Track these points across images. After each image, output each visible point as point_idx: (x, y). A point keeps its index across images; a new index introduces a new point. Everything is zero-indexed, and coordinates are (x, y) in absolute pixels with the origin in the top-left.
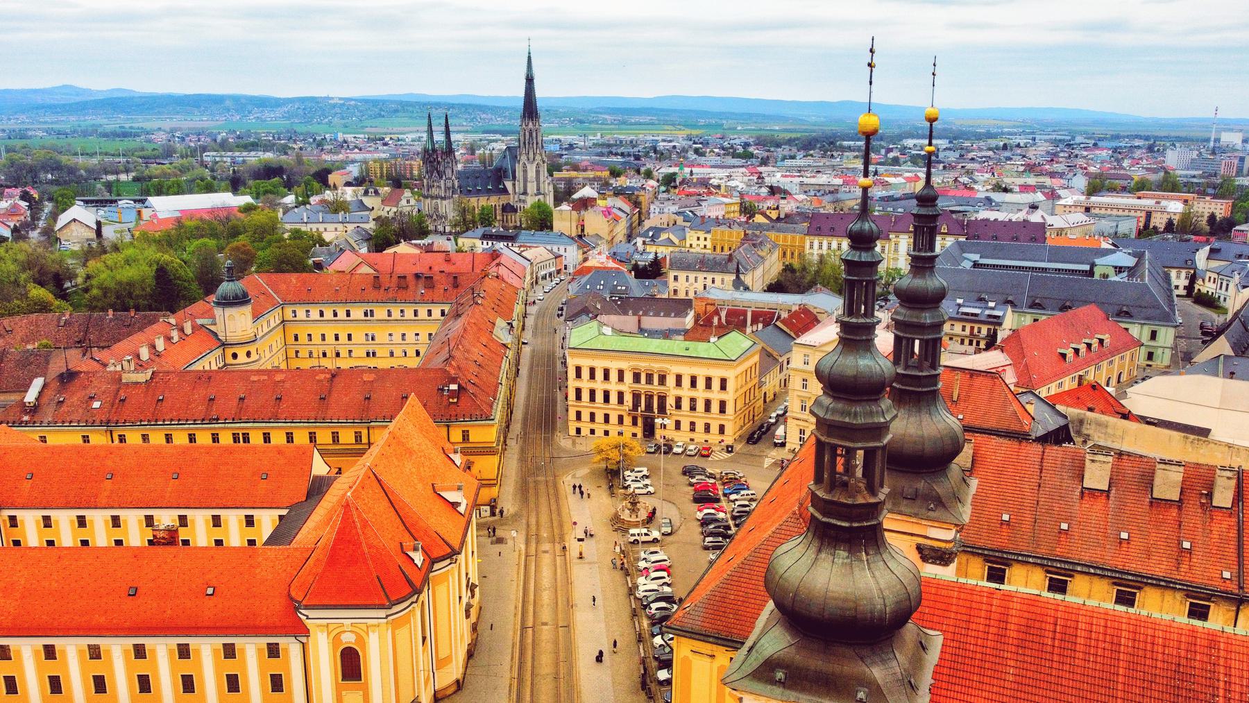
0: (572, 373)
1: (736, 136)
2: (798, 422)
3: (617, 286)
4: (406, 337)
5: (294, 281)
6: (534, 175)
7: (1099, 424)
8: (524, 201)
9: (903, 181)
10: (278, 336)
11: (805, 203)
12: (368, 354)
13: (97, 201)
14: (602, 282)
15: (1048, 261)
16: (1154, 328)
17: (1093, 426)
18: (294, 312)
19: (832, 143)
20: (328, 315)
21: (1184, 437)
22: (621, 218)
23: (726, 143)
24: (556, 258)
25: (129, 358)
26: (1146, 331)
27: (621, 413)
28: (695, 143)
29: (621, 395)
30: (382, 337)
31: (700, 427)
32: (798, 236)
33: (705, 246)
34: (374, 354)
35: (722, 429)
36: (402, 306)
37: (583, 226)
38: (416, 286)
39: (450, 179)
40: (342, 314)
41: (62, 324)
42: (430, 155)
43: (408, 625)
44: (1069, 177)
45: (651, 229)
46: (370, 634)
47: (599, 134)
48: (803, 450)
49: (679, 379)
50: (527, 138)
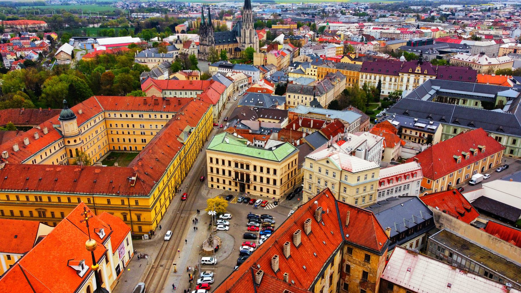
0: (208, 160)
1: (363, 3)
2: (307, 194)
3: (259, 101)
4: (158, 126)
5: (110, 100)
7: (448, 220)
8: (244, 46)
9: (430, 31)
10: (103, 124)
11: (376, 45)
12: (142, 133)
13: (80, 39)
14: (253, 99)
15: (474, 92)
16: (515, 138)
17: (445, 220)
18: (109, 114)
19: (407, 7)
20: (124, 116)
21: (489, 236)
22: (286, 54)
23: (357, 7)
24: (248, 78)
25: (5, 152)
26: (511, 140)
27: (231, 180)
28: (343, 7)
29: (230, 172)
30: (147, 126)
32: (356, 72)
33: (315, 74)
34: (144, 133)
35: (274, 192)
36: (156, 113)
37: (266, 60)
38: (163, 104)
39: (211, 37)
40: (130, 116)
41: (21, 113)
42: (202, 26)
44: (513, 29)
45: (295, 63)
47: (301, 3)
48: (264, 244)
50: (246, 17)
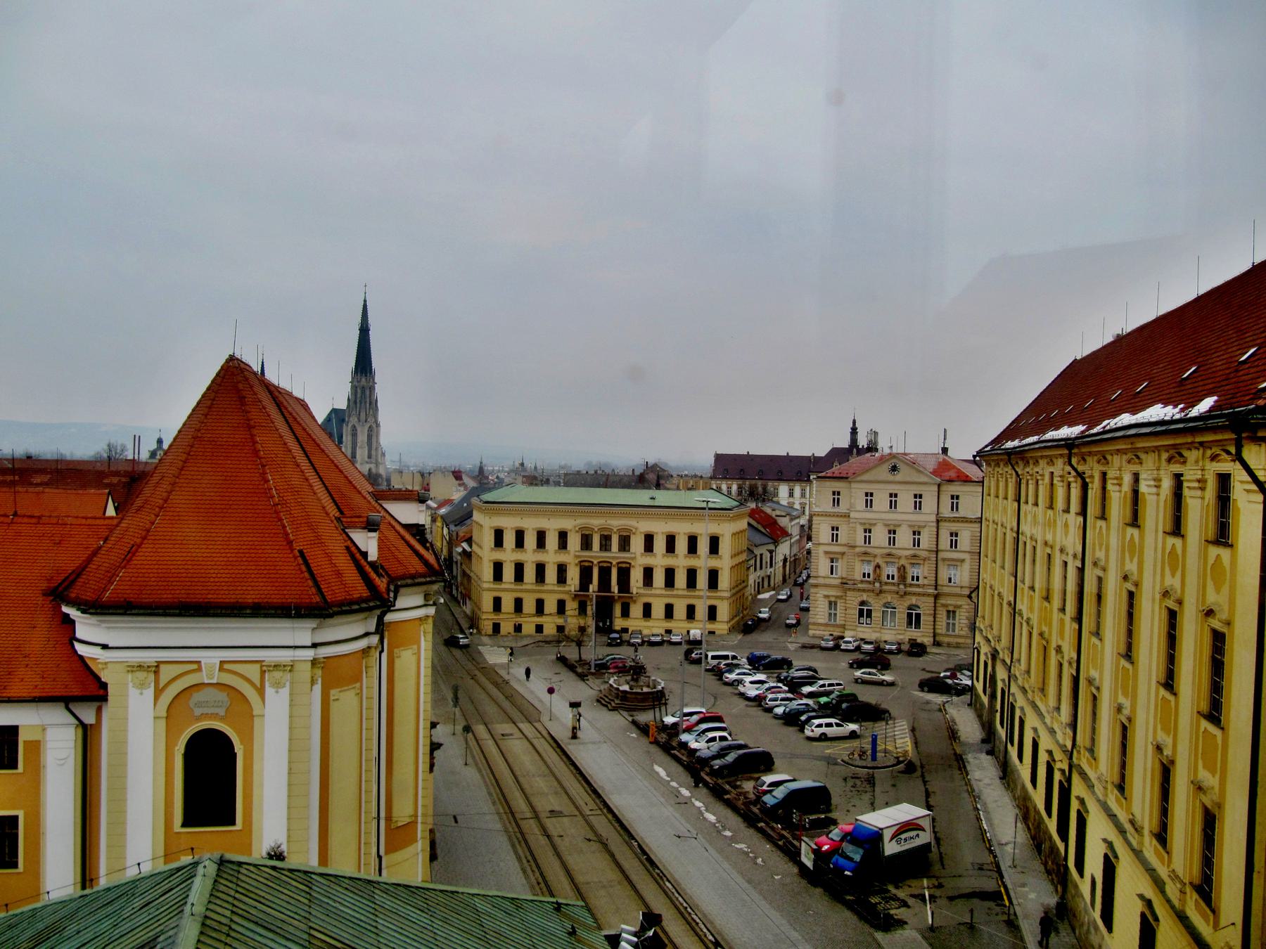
6: (366, 439)
29: (562, 570)
31: (680, 611)
35: (712, 613)
43: (358, 685)
46: (269, 691)
49: (649, 540)
50: (359, 396)
